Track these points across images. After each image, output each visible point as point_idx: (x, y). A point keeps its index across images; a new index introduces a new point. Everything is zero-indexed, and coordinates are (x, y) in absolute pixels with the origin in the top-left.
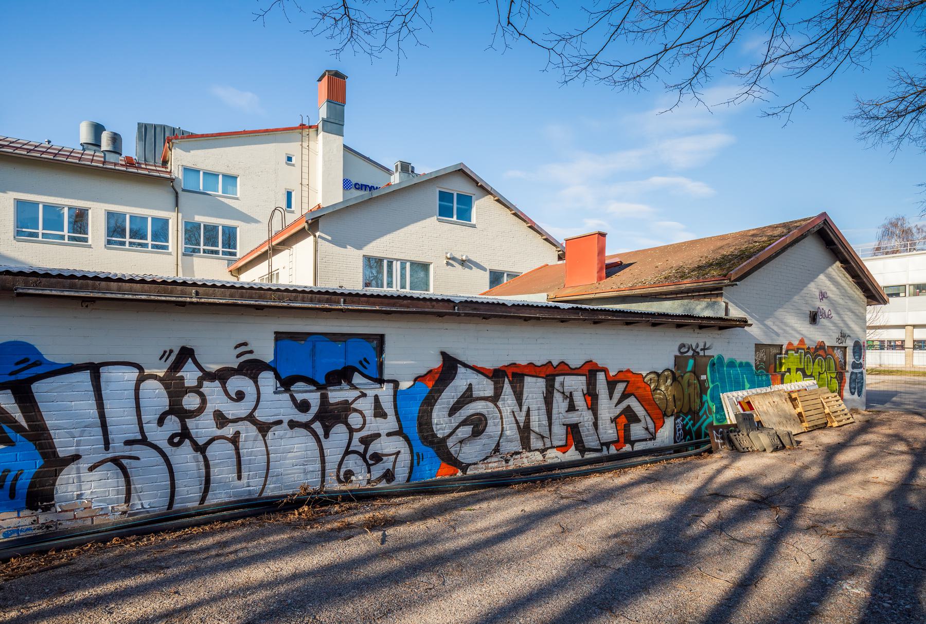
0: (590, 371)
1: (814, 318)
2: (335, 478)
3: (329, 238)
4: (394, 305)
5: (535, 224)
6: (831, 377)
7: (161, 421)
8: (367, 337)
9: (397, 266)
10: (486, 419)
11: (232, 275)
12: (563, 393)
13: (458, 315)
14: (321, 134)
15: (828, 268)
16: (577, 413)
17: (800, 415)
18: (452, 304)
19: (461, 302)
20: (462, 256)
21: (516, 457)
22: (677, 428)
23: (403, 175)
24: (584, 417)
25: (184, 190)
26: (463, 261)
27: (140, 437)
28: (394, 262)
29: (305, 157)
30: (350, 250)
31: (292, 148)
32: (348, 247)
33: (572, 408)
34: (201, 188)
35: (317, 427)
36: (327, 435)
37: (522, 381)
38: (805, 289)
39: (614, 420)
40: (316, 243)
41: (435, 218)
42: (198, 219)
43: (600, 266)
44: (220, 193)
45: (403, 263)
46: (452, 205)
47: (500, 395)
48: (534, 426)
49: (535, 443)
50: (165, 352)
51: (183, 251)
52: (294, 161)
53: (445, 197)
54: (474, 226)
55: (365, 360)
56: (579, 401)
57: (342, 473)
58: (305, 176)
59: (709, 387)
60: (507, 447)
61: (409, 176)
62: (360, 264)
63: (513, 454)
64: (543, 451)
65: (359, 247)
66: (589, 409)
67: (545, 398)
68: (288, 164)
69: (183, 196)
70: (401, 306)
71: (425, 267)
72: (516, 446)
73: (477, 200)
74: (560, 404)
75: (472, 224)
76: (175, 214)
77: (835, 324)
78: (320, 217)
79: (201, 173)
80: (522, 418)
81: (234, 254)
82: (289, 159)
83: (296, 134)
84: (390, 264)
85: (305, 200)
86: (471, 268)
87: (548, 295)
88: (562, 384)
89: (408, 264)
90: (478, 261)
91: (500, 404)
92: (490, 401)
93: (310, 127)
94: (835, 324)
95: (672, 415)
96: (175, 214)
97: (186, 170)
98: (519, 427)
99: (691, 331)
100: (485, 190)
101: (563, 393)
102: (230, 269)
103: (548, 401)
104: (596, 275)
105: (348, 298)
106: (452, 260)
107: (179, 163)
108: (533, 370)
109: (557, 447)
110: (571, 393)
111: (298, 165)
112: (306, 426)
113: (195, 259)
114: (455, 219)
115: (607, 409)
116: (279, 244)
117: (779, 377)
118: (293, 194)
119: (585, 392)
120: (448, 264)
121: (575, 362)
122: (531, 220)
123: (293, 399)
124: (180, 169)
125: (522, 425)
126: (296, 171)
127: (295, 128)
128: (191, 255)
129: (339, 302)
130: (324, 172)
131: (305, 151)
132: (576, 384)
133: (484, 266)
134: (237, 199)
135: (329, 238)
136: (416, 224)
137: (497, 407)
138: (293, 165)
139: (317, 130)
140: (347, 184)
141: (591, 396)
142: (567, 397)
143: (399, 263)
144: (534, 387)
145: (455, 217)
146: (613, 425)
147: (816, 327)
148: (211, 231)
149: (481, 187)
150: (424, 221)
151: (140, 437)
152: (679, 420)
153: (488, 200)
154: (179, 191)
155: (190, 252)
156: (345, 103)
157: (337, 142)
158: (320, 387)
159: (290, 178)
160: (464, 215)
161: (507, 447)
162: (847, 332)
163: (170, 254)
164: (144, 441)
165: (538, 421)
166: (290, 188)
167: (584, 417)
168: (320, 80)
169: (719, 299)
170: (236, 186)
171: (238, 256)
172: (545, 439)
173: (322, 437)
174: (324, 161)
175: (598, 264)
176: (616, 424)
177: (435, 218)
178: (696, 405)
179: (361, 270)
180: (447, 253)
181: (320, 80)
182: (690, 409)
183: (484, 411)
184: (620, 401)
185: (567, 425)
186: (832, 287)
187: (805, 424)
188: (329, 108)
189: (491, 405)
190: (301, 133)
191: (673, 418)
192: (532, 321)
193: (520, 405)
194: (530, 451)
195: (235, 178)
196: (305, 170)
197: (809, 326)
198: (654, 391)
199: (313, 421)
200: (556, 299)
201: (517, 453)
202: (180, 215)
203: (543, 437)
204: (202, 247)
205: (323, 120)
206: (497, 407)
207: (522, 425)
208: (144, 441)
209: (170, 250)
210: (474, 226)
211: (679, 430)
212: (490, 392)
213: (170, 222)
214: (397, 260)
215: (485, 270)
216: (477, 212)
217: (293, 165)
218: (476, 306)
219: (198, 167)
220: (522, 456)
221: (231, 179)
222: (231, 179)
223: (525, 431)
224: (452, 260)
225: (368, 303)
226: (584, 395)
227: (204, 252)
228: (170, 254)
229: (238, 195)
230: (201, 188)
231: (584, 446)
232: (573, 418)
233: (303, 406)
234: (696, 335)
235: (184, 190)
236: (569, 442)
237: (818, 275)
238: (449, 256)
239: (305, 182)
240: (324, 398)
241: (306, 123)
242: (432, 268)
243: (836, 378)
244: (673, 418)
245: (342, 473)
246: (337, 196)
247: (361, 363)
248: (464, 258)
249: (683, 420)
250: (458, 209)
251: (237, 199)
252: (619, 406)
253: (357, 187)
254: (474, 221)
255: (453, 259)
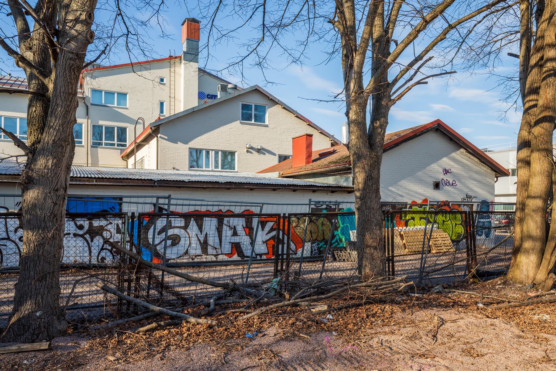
0: (248, 216)
1: (437, 186)
2: (96, 260)
3: (166, 138)
4: (122, 182)
5: (312, 123)
6: (456, 224)
7: (16, 231)
8: (115, 198)
9: (212, 154)
10: (180, 238)
11: (123, 160)
12: (229, 226)
13: (156, 186)
14: (183, 62)
15: (451, 153)
16: (238, 237)
17: (404, 244)
18: (153, 181)
19: (158, 180)
20: (258, 146)
21: (199, 257)
22: (313, 249)
23: (222, 93)
24: (244, 240)
25: (92, 104)
26: (259, 149)
27: (7, 237)
28: (210, 152)
29: (172, 79)
30: (180, 144)
31: (163, 72)
32: (179, 143)
33: (235, 234)
34: (103, 102)
35: (87, 236)
36: (92, 241)
37: (202, 220)
38: (428, 167)
39: (266, 242)
40: (158, 140)
41: (239, 121)
42: (101, 123)
43: (308, 155)
44: (116, 105)
45: (217, 152)
46: (251, 112)
47: (188, 226)
48: (211, 241)
49: (210, 250)
50: (18, 203)
51: (92, 144)
52: (165, 81)
53: (245, 107)
54: (267, 126)
55: (113, 207)
56: (240, 230)
57: (100, 258)
58: (172, 91)
59: (340, 227)
60: (192, 252)
61: (226, 94)
62: (187, 153)
63: (197, 256)
64: (216, 256)
65: (186, 142)
66: (247, 235)
67: (217, 229)
68: (161, 84)
69: (91, 108)
70: (125, 183)
71: (232, 154)
72: (199, 252)
73: (269, 108)
74: (227, 232)
75: (266, 125)
76: (86, 120)
77: (459, 190)
78: (160, 125)
79: (103, 92)
80: (202, 239)
81: (125, 145)
82: (162, 80)
83: (166, 63)
84: (208, 152)
85: (172, 108)
86: (264, 154)
87: (279, 173)
88: (229, 222)
89: (220, 153)
90: (270, 149)
91: (188, 230)
92: (183, 229)
93: (176, 58)
94: (459, 190)
95: (309, 241)
96: (86, 120)
97: (94, 91)
98: (200, 242)
99: (326, 194)
100: (274, 102)
101: (229, 226)
102: (122, 155)
103: (219, 230)
104: (305, 160)
105: (97, 180)
106: (251, 149)
107: (89, 87)
108: (209, 214)
109: (225, 254)
110: (235, 227)
111: (168, 84)
112: (82, 236)
113: (99, 149)
114: (253, 122)
115: (262, 236)
116: (143, 141)
117: (403, 222)
118: (165, 104)
119: (244, 226)
120: (248, 151)
121: (238, 210)
122: (309, 121)
123: (76, 224)
124: (90, 90)
125: (202, 241)
126: (166, 88)
127: (166, 59)
128: (97, 147)
129: (93, 181)
130: (185, 88)
131: (172, 74)
132: (240, 223)
133: (274, 152)
134: (127, 109)
135: (166, 138)
136: (225, 127)
137: (187, 232)
138: (164, 84)
139: (181, 59)
140: (201, 95)
141: (249, 229)
142: (232, 228)
143: (213, 152)
144: (210, 224)
145: (253, 120)
146: (265, 245)
147: (438, 191)
148: (110, 130)
149: (271, 99)
150: (231, 124)
151: (7, 237)
152: (314, 245)
153: (276, 109)
154: (89, 105)
155: (96, 145)
156: (199, 40)
157: (194, 66)
158: (89, 219)
159: (162, 94)
160: (260, 119)
161: (192, 252)
162: (470, 194)
163: (83, 146)
164: (8, 239)
165: (213, 240)
166: (162, 99)
167: (244, 240)
168: (183, 25)
169: (350, 175)
170: (126, 100)
171: (127, 146)
172: (217, 250)
173: (90, 242)
174: (185, 81)
175: (306, 154)
176: (266, 244)
177: (239, 121)
178: (328, 236)
179: (188, 157)
180: (247, 145)
181: (183, 25)
182: (324, 239)
183: (178, 234)
184: (269, 232)
185: (232, 243)
186: (456, 165)
187: (407, 250)
188: (188, 44)
189: (183, 231)
190: (170, 62)
191: (309, 243)
192: (256, 189)
193: (201, 232)
194: (207, 255)
195: (125, 95)
196: (172, 87)
197: (433, 191)
198: (295, 227)
199: (85, 234)
200: (283, 176)
201: (199, 256)
202: (89, 121)
203: (216, 248)
204: (104, 141)
205: (184, 53)
206: (187, 232)
207: (202, 241)
208: (8, 239)
209: (83, 144)
210: (267, 126)
211: (315, 250)
212: (183, 224)
213: (83, 125)
214: (212, 150)
215: (275, 155)
216: (269, 117)
217: (164, 84)
218: (168, 182)
219: (102, 88)
220: (203, 257)
221: (123, 95)
222: (123, 95)
223: (204, 245)
224: (251, 149)
225: (108, 182)
226: (244, 228)
227: (106, 144)
228: (83, 146)
229: (128, 106)
230: (103, 102)
231: (243, 255)
232: (236, 239)
233: (81, 227)
234: (329, 196)
235: (92, 104)
236: (234, 252)
237: (442, 158)
238: (248, 146)
239: (172, 95)
240: (91, 225)
241: (173, 55)
242: (236, 154)
243: (461, 224)
244: (309, 243)
245: (100, 258)
246: (194, 103)
247: (110, 208)
248: (259, 147)
249: (318, 244)
250: (255, 115)
251: (127, 109)
252: (269, 235)
253: (209, 97)
254: (267, 122)
255: (252, 148)
